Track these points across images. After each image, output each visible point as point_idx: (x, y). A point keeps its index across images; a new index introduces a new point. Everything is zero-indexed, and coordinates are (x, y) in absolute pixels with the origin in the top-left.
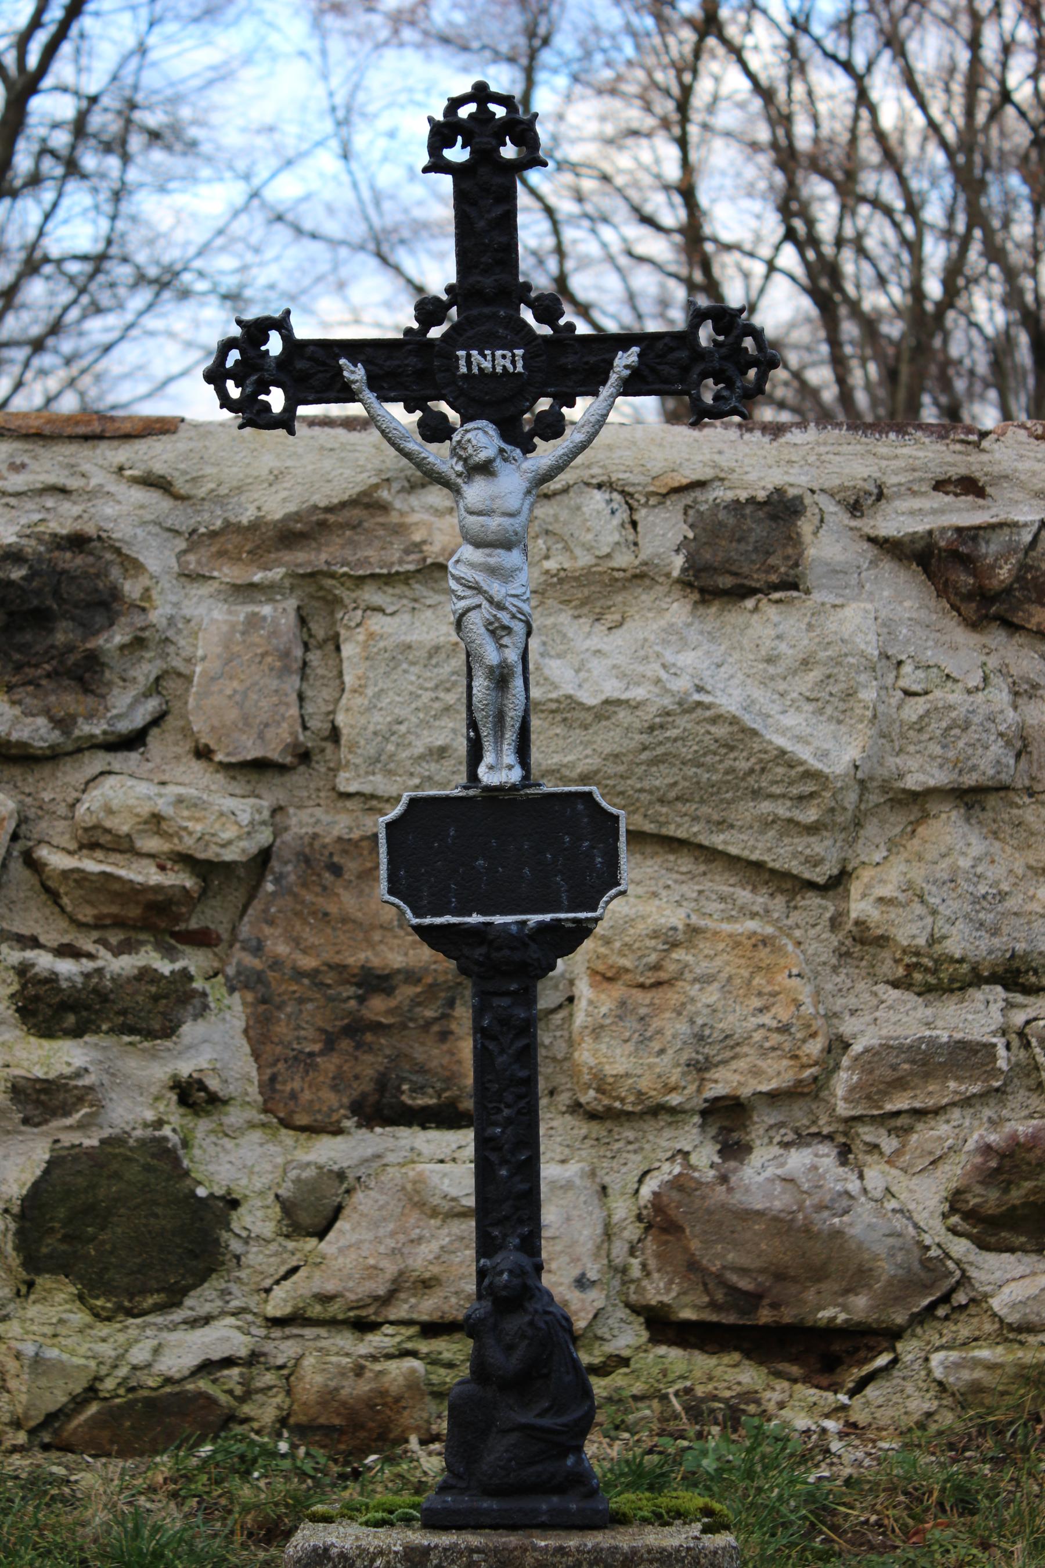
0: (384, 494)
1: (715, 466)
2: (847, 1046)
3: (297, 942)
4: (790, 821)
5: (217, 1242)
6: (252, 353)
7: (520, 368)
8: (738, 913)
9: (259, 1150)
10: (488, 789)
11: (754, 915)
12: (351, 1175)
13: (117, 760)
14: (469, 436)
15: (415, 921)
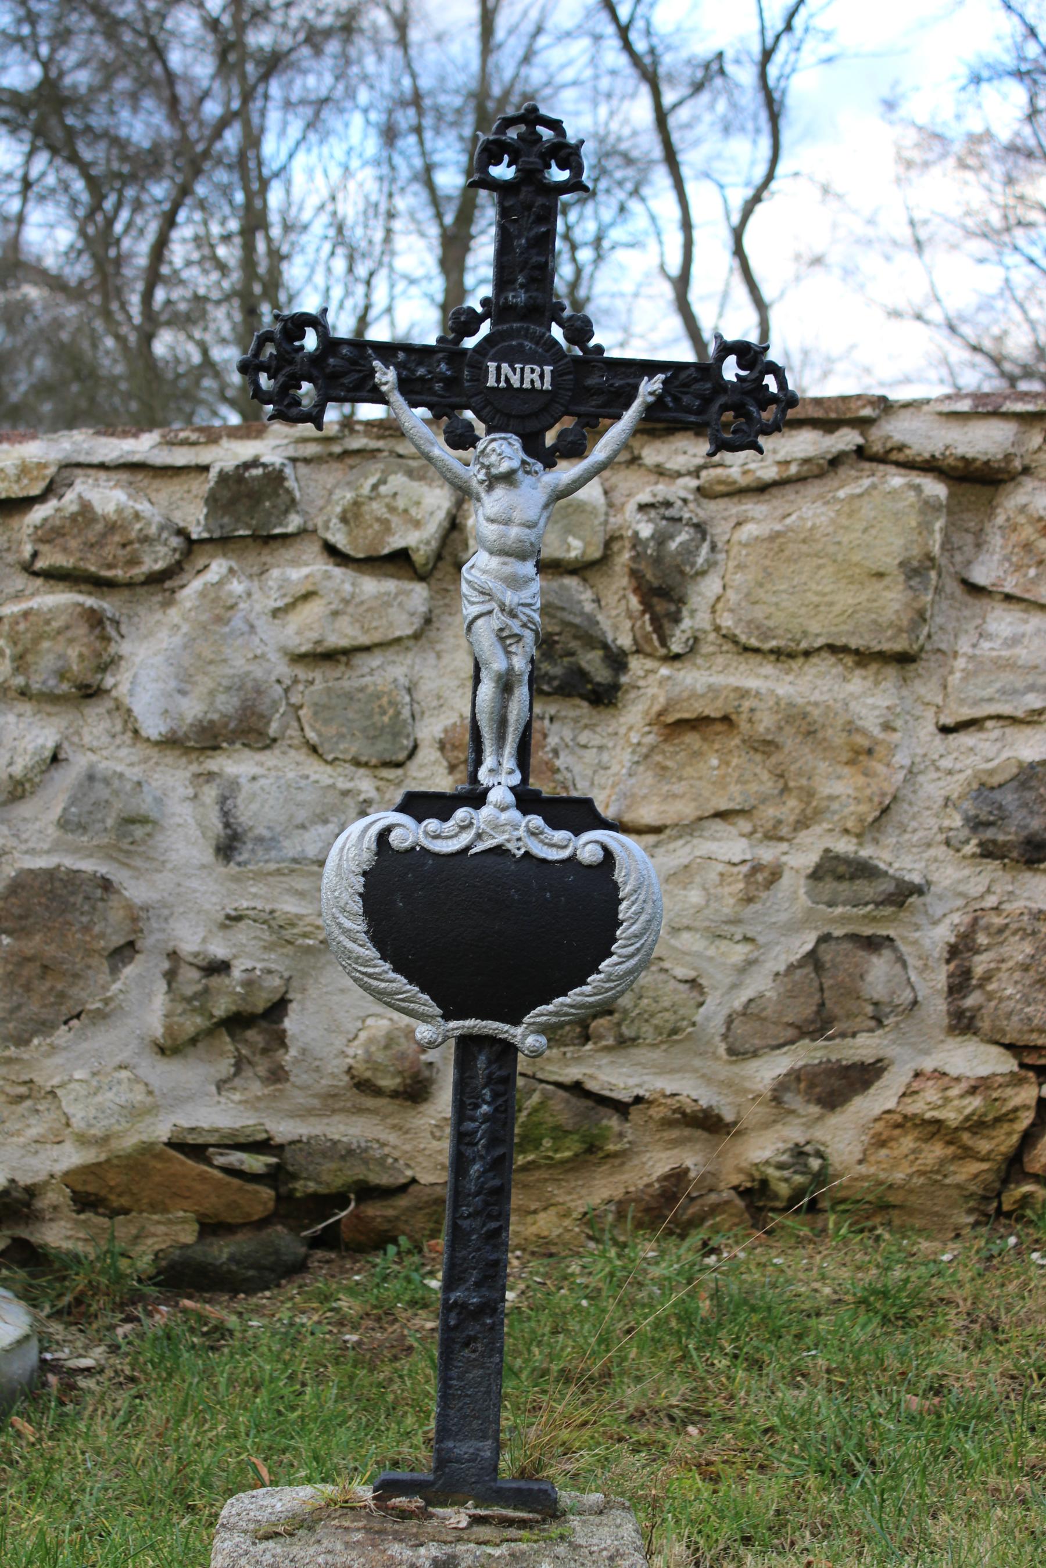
7: (547, 386)
14: (494, 445)
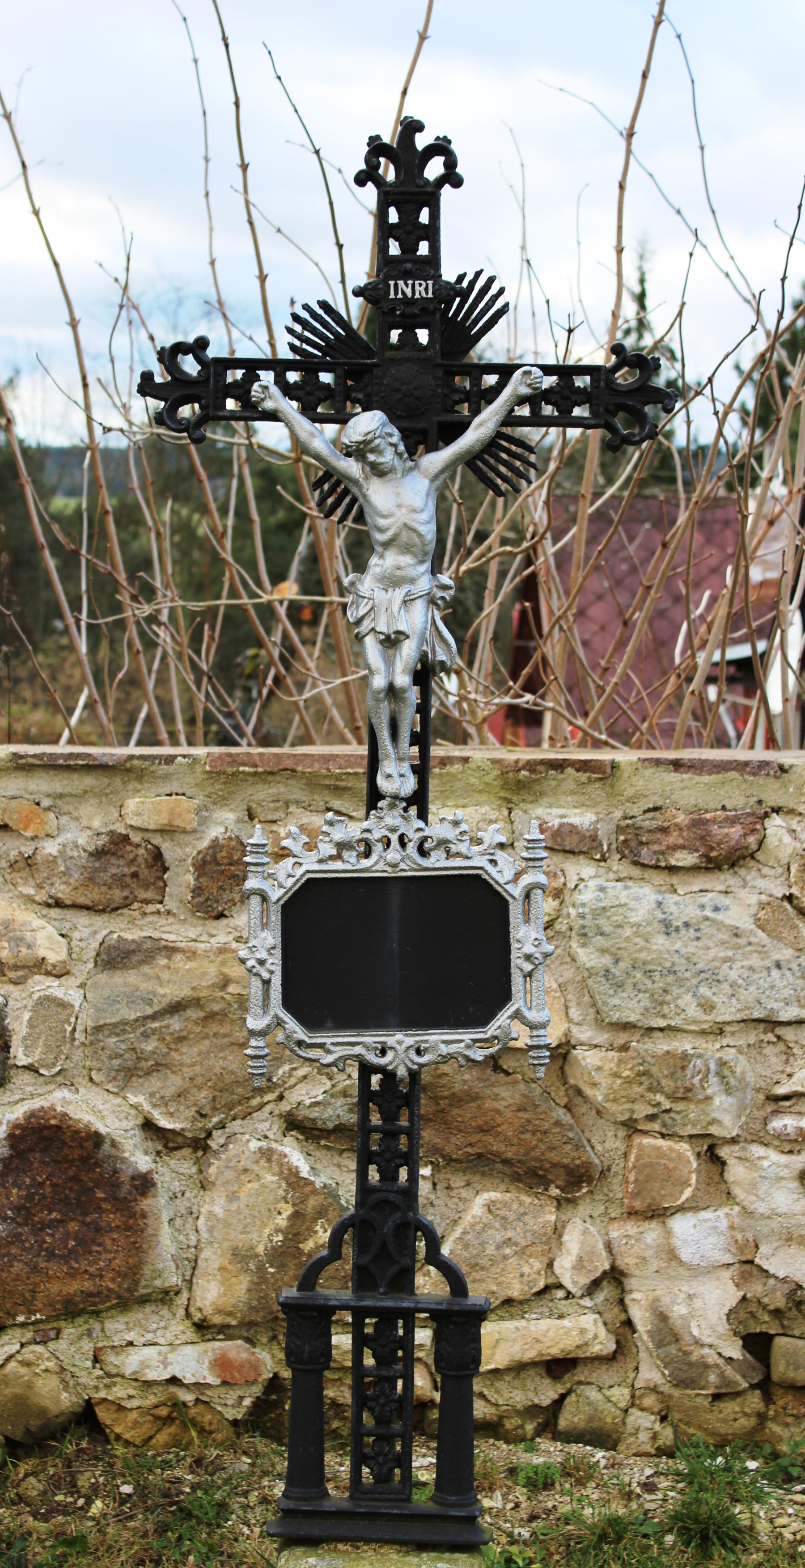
7: (430, 295)
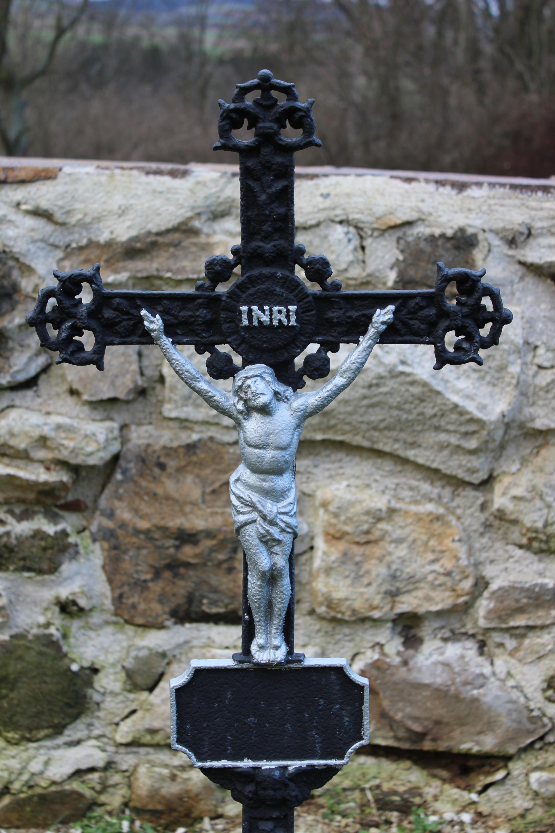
0: (197, 224)
1: (420, 211)
2: (487, 585)
3: (136, 511)
4: (458, 447)
5: (85, 696)
6: (67, 303)
7: (293, 322)
8: (422, 500)
9: (112, 638)
10: (258, 664)
11: (431, 500)
12: (170, 654)
13: (18, 398)
14: (249, 382)
15: (200, 764)
